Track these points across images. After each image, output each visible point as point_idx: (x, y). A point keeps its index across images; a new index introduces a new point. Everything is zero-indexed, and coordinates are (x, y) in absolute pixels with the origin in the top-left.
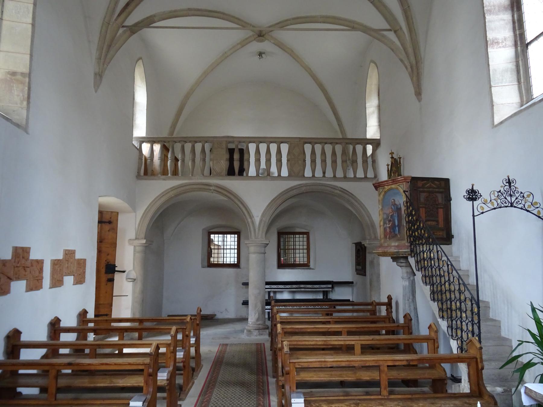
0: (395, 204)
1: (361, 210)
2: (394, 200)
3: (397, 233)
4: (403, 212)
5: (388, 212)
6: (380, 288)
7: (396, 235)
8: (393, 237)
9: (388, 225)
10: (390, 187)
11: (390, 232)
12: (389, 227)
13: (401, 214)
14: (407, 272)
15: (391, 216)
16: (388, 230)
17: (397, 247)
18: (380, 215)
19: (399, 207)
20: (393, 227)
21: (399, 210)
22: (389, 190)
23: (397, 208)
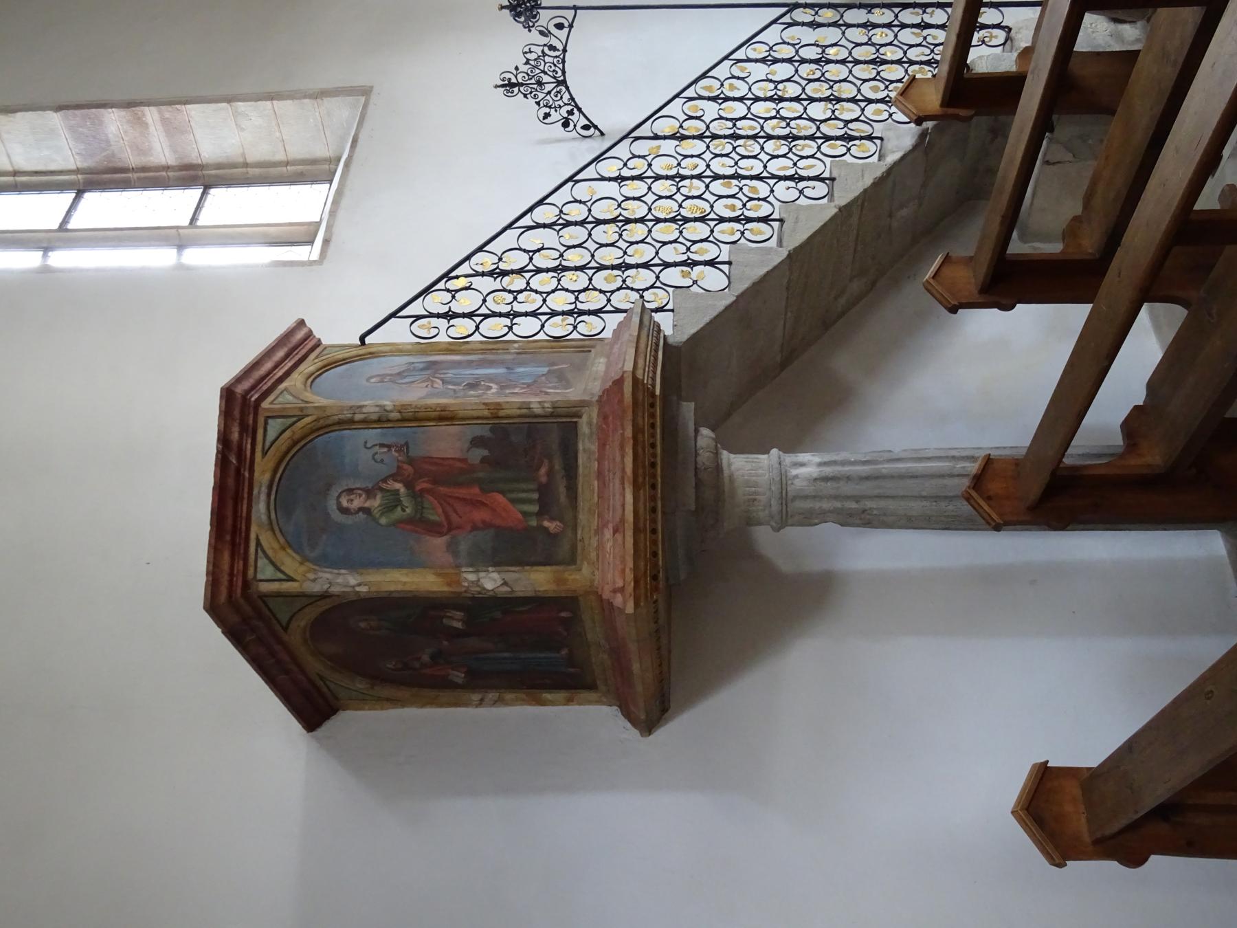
1: (246, 495)
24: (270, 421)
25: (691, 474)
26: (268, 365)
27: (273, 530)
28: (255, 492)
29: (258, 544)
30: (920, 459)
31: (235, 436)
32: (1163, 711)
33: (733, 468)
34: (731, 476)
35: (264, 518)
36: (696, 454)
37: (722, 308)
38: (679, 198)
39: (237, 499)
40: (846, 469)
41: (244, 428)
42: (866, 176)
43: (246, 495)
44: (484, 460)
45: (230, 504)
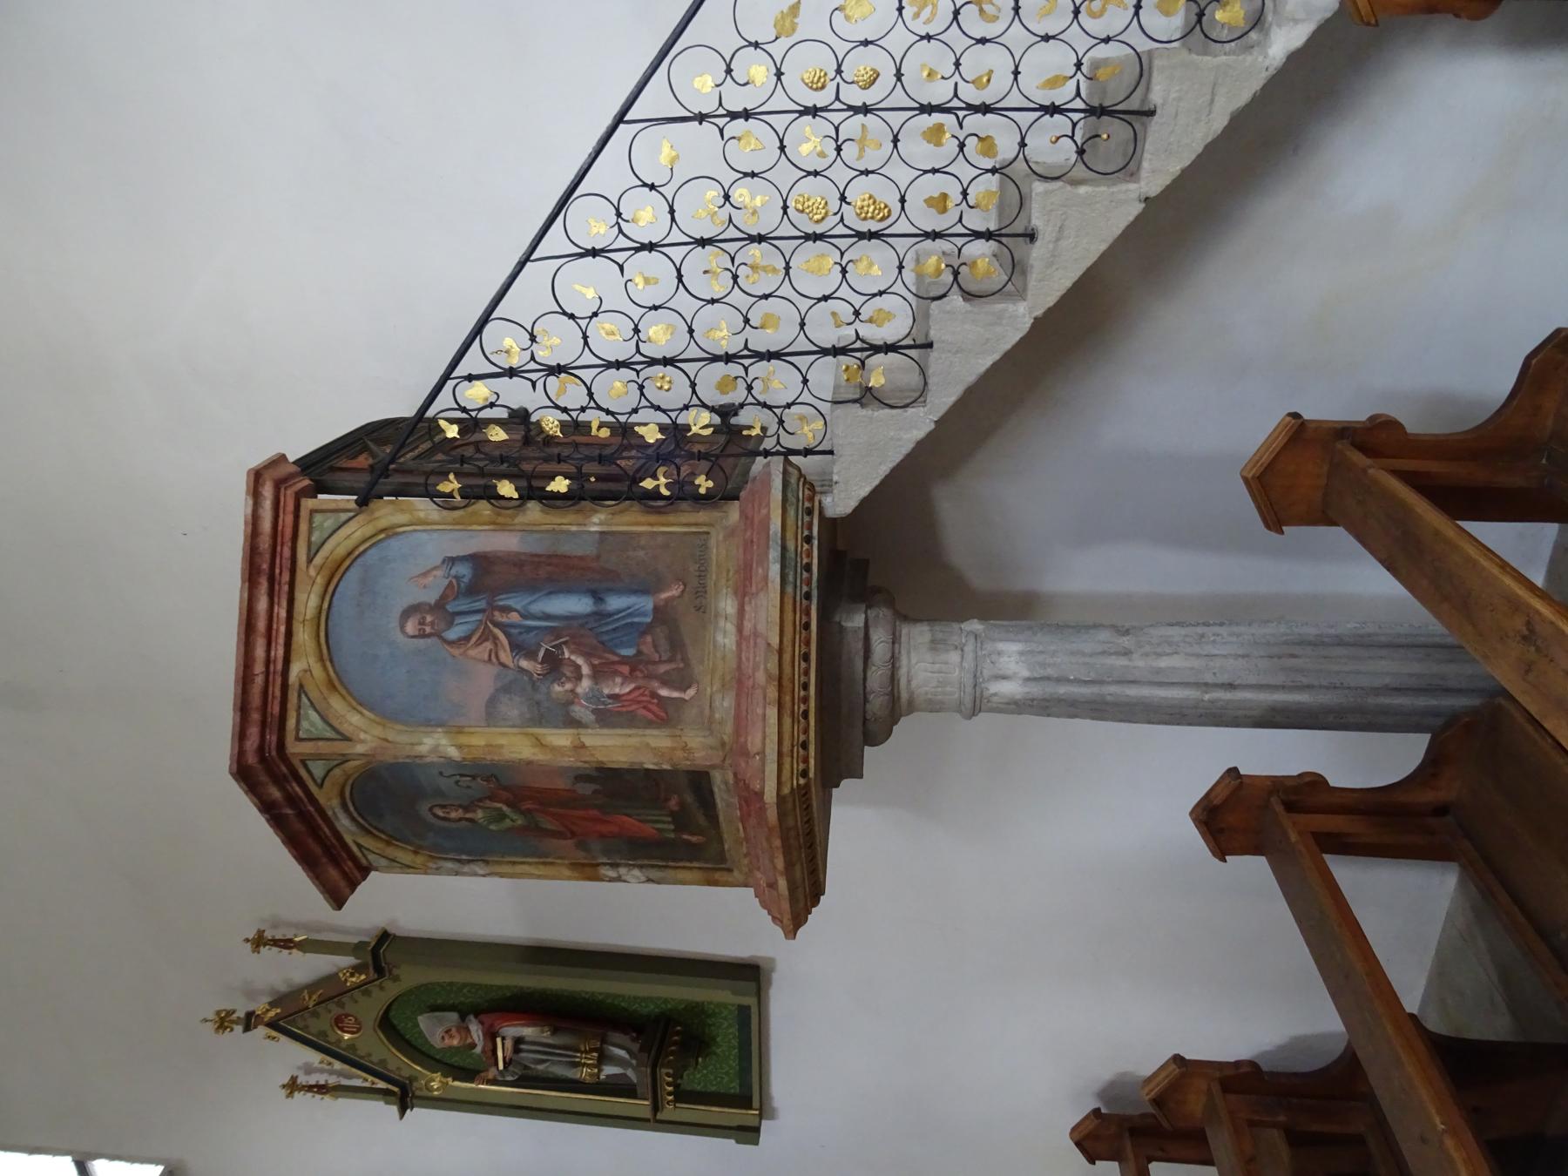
0: (439, 606)
1: (320, 821)
2: (407, 613)
3: (646, 603)
4: (505, 542)
5: (484, 679)
6: (1206, 147)
7: (662, 614)
8: (676, 646)
9: (586, 684)
10: (303, 636)
11: (635, 665)
12: (598, 674)
13: (517, 562)
14: (935, 645)
15: (517, 648)
16: (618, 687)
17: (743, 592)
18: (619, 879)
19: (464, 570)
20: (593, 635)
21: (485, 577)
22: (327, 651)
23: (472, 590)
24: (301, 735)
25: (859, 724)
26: (260, 652)
27: (370, 833)
28: (330, 813)
29: (359, 846)
30: (1160, 684)
31: (276, 793)
32: (1333, 996)
33: (914, 684)
34: (911, 694)
35: (354, 828)
36: (866, 700)
37: (911, 446)
38: (841, 174)
39: (314, 831)
40: (1062, 690)
41: (279, 781)
42: (1220, 101)
43: (320, 821)
44: (595, 792)
45: (311, 842)
